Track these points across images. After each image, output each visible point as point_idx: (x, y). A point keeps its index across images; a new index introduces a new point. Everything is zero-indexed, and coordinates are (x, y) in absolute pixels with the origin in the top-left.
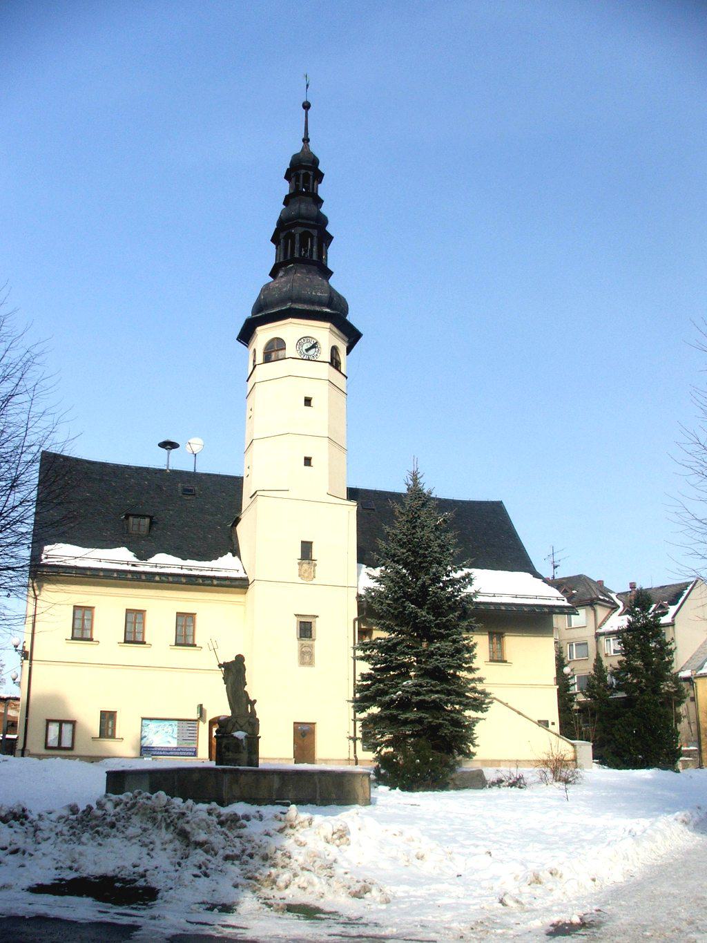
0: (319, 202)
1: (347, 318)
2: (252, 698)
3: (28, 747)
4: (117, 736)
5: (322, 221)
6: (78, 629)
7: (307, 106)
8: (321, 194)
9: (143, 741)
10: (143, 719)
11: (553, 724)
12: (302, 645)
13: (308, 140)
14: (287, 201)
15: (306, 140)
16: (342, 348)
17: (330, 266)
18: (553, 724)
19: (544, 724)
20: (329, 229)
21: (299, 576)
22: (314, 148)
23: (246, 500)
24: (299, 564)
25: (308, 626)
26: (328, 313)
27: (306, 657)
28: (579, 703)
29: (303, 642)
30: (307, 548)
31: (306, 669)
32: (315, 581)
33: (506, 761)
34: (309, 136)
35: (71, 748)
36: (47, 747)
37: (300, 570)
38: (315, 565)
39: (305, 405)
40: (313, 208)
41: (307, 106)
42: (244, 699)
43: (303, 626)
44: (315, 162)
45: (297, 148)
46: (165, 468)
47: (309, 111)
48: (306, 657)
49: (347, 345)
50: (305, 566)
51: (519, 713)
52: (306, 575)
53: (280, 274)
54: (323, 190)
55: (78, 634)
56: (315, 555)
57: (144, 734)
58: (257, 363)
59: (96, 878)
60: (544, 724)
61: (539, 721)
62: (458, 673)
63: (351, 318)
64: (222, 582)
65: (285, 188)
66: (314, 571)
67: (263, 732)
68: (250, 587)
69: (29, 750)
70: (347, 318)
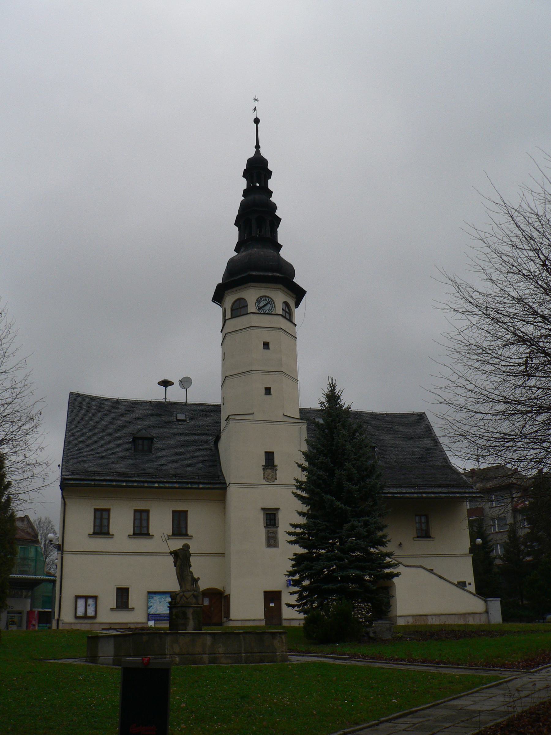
0: (270, 193)
1: (294, 280)
2: (196, 576)
3: (62, 617)
4: (130, 607)
6: (137, 527)
7: (257, 121)
8: (270, 187)
9: (149, 610)
10: (149, 593)
11: (470, 584)
13: (259, 147)
15: (257, 147)
16: (292, 304)
18: (470, 584)
19: (462, 585)
20: (270, 167)
21: (264, 478)
22: (264, 153)
23: (223, 423)
24: (263, 469)
25: (272, 517)
26: (278, 276)
28: (498, 566)
29: (269, 529)
30: (269, 456)
31: (272, 550)
32: (276, 482)
33: (445, 615)
34: (260, 144)
35: (95, 617)
36: (76, 617)
37: (264, 474)
38: (276, 470)
39: (264, 349)
40: (270, 252)
41: (257, 121)
42: (189, 578)
43: (268, 516)
44: (265, 162)
45: (251, 153)
46: (164, 401)
49: (295, 300)
50: (269, 471)
51: (441, 577)
52: (269, 477)
53: (242, 250)
54: (272, 184)
55: (137, 532)
56: (276, 462)
57: (150, 604)
58: (227, 318)
60: (462, 585)
61: (459, 583)
62: (306, 551)
63: (298, 280)
64: (142, 485)
65: (243, 184)
66: (276, 474)
68: (228, 489)
69: (63, 620)
70: (294, 280)
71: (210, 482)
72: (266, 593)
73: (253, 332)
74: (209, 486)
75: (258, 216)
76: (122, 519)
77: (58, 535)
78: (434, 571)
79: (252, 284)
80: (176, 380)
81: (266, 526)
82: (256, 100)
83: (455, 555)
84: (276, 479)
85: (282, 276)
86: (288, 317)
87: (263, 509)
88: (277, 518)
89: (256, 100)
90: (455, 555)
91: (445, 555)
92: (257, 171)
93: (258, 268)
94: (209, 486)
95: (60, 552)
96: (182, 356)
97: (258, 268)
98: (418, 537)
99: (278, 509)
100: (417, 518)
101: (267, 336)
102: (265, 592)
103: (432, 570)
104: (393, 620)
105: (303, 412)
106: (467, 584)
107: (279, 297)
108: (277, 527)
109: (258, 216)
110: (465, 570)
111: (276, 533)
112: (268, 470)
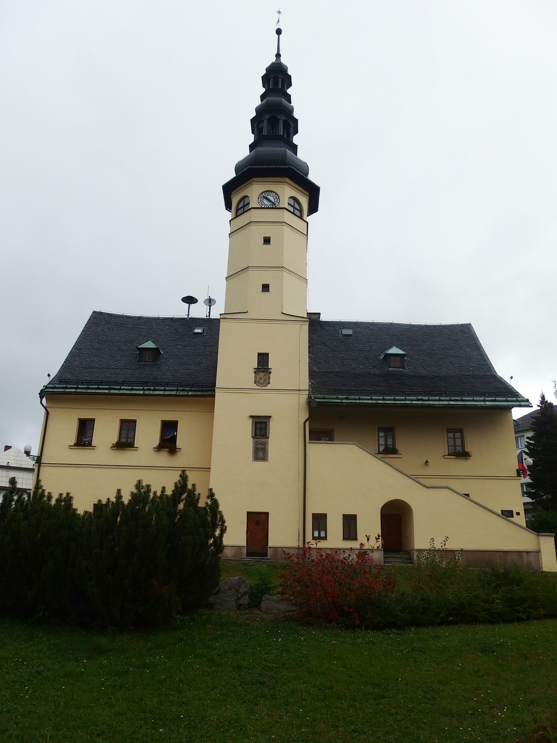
5: (289, 112)
7: (279, 32)
11: (518, 514)
12: (257, 442)
14: (263, 97)
15: (278, 55)
17: (526, 398)
18: (518, 514)
21: (255, 383)
24: (255, 372)
27: (260, 453)
30: (263, 358)
31: (260, 464)
37: (256, 377)
38: (270, 373)
41: (279, 32)
47: (274, 59)
48: (260, 453)
50: (262, 374)
52: (261, 381)
59: (538, 414)
60: (508, 514)
61: (503, 512)
63: (312, 177)
66: (269, 377)
67: (223, 514)
71: (201, 388)
72: (345, 517)
73: (253, 227)
74: (199, 393)
75: (275, 120)
76: (106, 430)
78: (471, 497)
79: (255, 179)
80: (201, 298)
81: (255, 436)
82: (279, 12)
83: (498, 478)
84: (269, 383)
86: (299, 214)
87: (251, 417)
88: (268, 427)
89: (279, 12)
90: (498, 478)
92: (277, 79)
94: (199, 393)
95: (37, 464)
96: (173, 256)
98: (449, 455)
99: (270, 417)
100: (451, 435)
101: (267, 231)
102: (248, 513)
103: (468, 495)
104: (408, 554)
107: (286, 191)
108: (268, 438)
110: (514, 497)
111: (265, 444)
112: (260, 373)
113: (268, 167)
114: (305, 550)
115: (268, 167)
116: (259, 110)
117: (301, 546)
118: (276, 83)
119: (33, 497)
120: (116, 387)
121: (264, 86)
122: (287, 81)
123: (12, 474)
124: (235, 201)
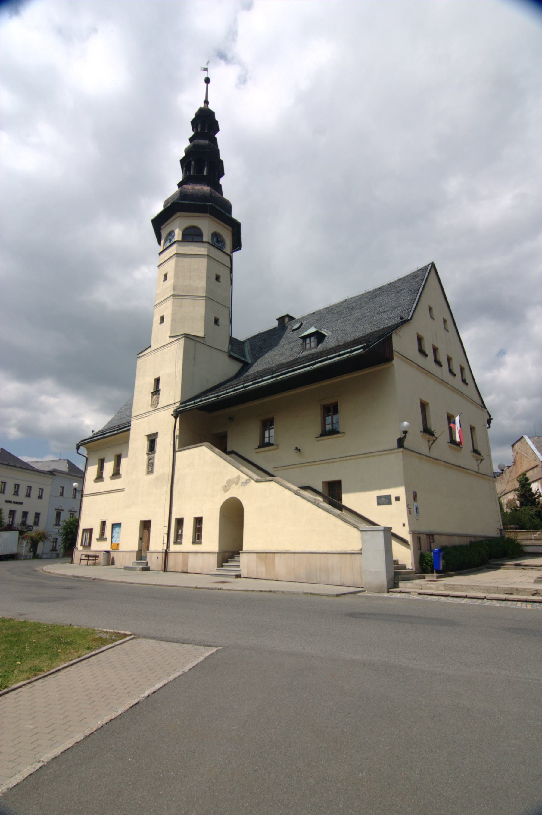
7: (207, 81)
14: (191, 140)
15: (206, 102)
18: (397, 499)
22: (205, 85)
34: (209, 100)
41: (207, 81)
47: (209, 85)
63: (235, 215)
72: (379, 504)
74: (115, 432)
75: (203, 159)
77: (35, 528)
85: (221, 210)
91: (367, 454)
93: (201, 205)
97: (201, 205)
105: (233, 341)
106: (393, 499)
107: (207, 225)
109: (203, 159)
113: (203, 203)
114: (502, 537)
115: (203, 203)
116: (188, 152)
117: (499, 535)
118: (203, 128)
119: (37, 457)
120: (259, 380)
121: (193, 131)
122: (214, 127)
123: (429, 454)
124: (164, 234)
